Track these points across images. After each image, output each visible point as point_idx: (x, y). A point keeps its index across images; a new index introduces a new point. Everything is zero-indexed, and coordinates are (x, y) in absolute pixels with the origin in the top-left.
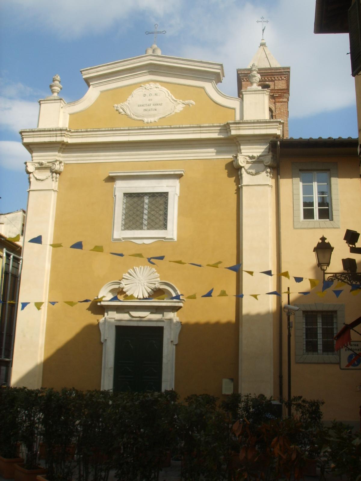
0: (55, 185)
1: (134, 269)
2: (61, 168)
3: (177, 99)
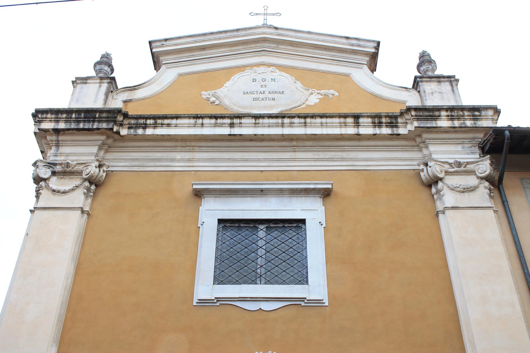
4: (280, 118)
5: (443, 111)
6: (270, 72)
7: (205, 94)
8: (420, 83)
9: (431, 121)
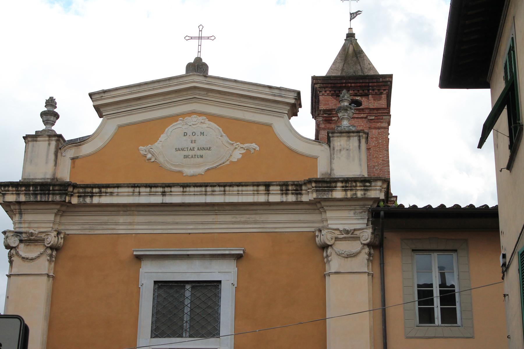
2: (59, 242)
4: (203, 187)
5: (339, 183)
6: (199, 123)
7: (142, 149)
8: (331, 139)
9: (328, 192)
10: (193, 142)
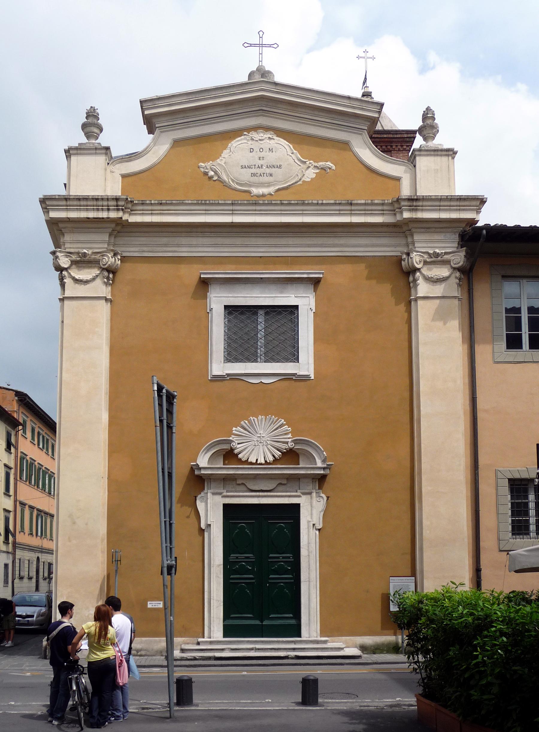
0: (105, 291)
1: (250, 422)
3: (306, 159)
10: (261, 159)
